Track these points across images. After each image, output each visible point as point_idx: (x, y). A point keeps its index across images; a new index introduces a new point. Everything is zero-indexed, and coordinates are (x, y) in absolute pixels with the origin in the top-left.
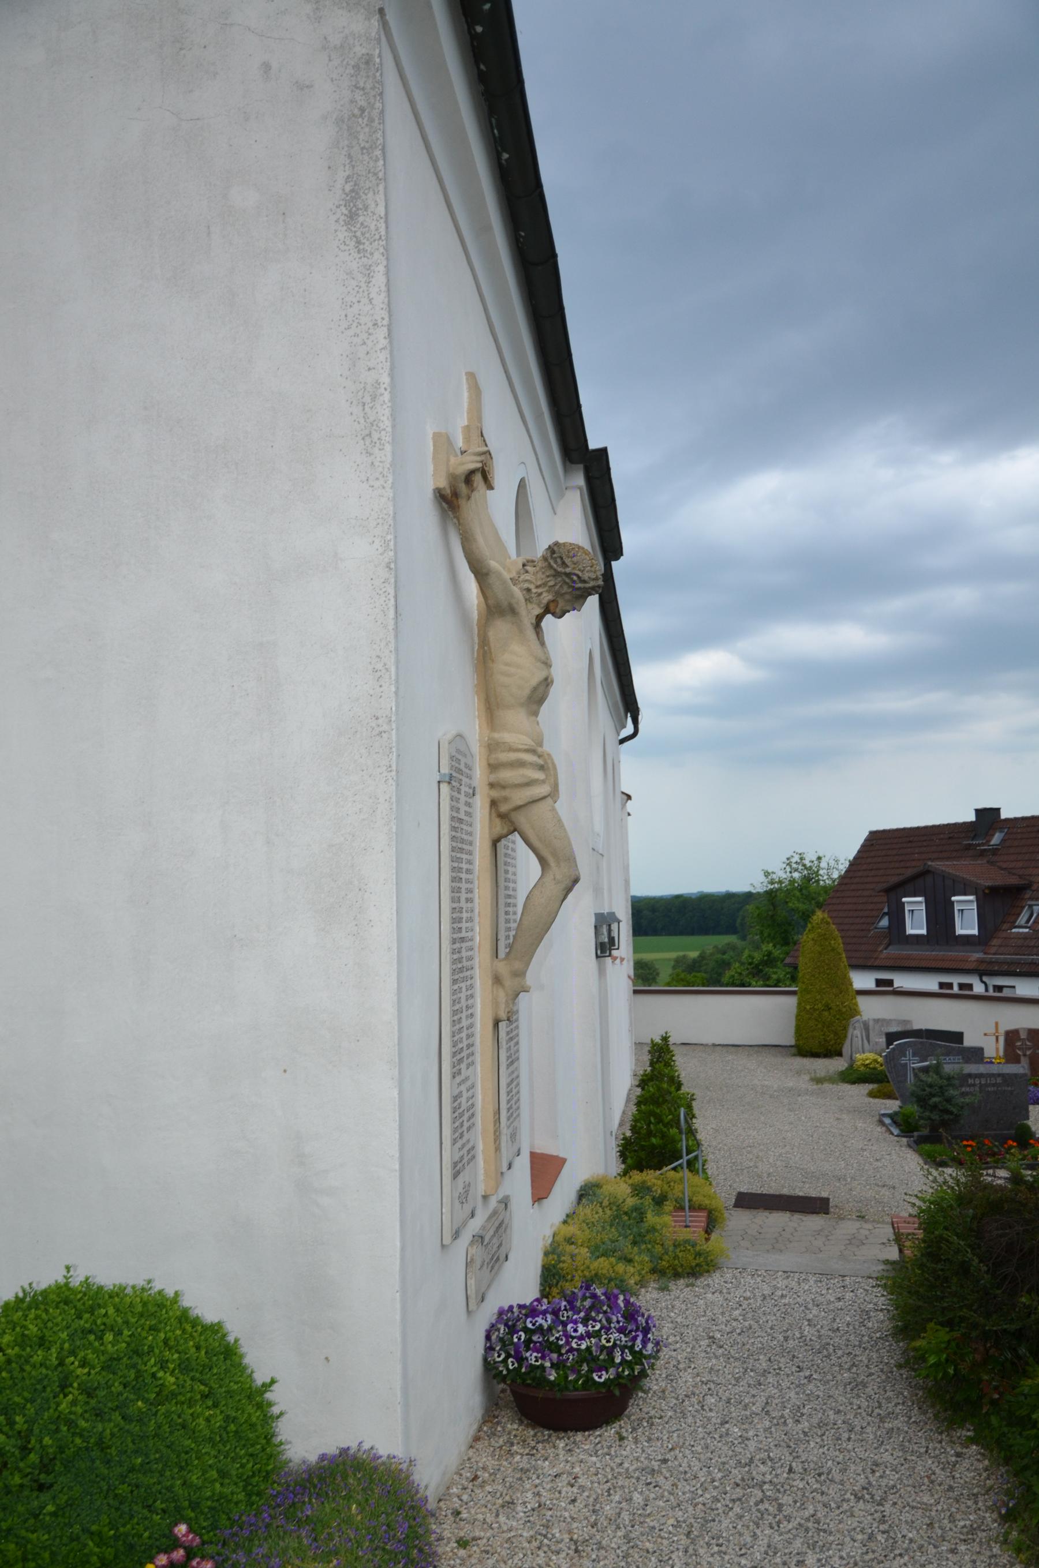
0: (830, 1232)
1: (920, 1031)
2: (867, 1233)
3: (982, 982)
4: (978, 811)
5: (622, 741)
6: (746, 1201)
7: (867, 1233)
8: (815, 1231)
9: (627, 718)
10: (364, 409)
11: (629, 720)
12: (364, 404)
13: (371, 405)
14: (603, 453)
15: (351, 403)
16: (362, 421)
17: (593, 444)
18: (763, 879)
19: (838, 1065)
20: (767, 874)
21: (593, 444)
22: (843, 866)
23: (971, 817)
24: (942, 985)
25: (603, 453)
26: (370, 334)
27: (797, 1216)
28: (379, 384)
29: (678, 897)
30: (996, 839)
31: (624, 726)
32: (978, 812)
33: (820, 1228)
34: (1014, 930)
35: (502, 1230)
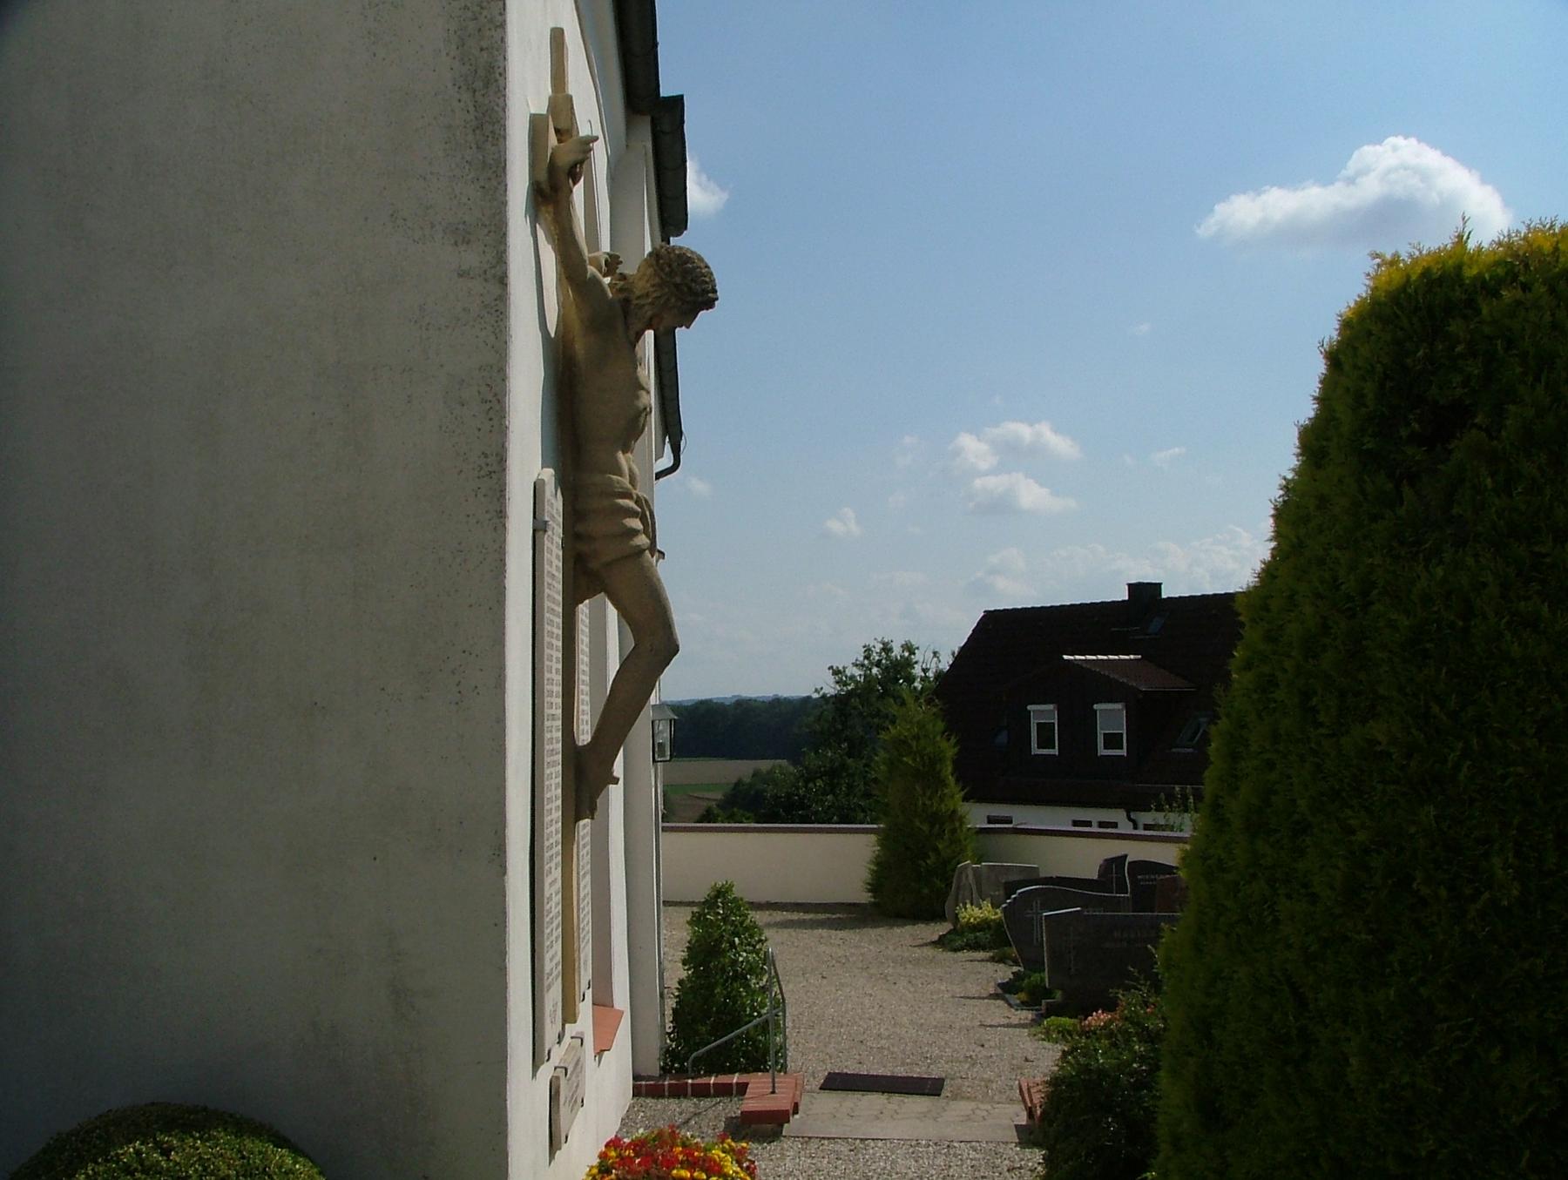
0: (938, 1114)
1: (1046, 878)
2: (985, 1113)
3: (1130, 819)
4: (1130, 586)
5: (659, 475)
6: (838, 1083)
7: (985, 1113)
8: (921, 1113)
9: (664, 444)
10: (474, 96)
11: (668, 448)
12: (475, 91)
13: (483, 92)
14: (677, 102)
15: (459, 88)
16: (472, 109)
17: (666, 91)
18: (831, 679)
19: (942, 928)
20: (836, 672)
21: (666, 91)
22: (945, 663)
23: (1124, 596)
24: (1075, 823)
25: (677, 102)
26: (482, 8)
27: (896, 1098)
28: (493, 68)
29: (702, 702)
30: (1156, 624)
31: (660, 455)
32: (1133, 588)
33: (925, 1110)
34: (1174, 750)
35: (578, 1069)
